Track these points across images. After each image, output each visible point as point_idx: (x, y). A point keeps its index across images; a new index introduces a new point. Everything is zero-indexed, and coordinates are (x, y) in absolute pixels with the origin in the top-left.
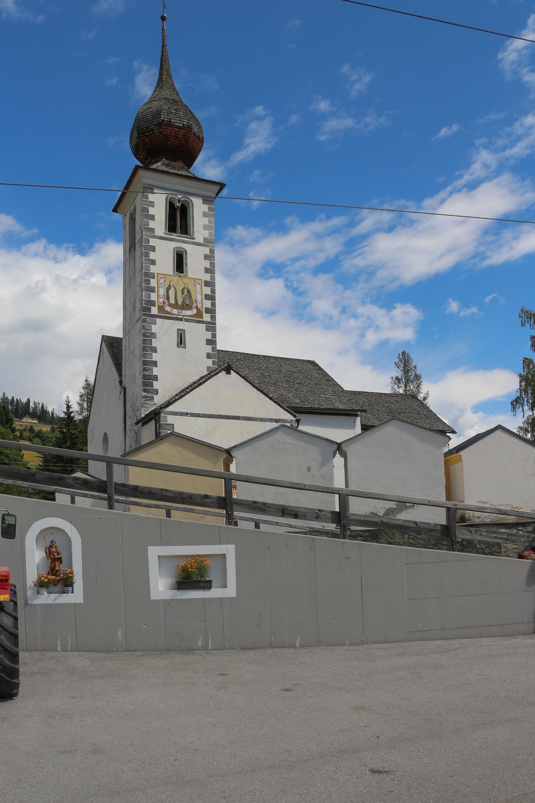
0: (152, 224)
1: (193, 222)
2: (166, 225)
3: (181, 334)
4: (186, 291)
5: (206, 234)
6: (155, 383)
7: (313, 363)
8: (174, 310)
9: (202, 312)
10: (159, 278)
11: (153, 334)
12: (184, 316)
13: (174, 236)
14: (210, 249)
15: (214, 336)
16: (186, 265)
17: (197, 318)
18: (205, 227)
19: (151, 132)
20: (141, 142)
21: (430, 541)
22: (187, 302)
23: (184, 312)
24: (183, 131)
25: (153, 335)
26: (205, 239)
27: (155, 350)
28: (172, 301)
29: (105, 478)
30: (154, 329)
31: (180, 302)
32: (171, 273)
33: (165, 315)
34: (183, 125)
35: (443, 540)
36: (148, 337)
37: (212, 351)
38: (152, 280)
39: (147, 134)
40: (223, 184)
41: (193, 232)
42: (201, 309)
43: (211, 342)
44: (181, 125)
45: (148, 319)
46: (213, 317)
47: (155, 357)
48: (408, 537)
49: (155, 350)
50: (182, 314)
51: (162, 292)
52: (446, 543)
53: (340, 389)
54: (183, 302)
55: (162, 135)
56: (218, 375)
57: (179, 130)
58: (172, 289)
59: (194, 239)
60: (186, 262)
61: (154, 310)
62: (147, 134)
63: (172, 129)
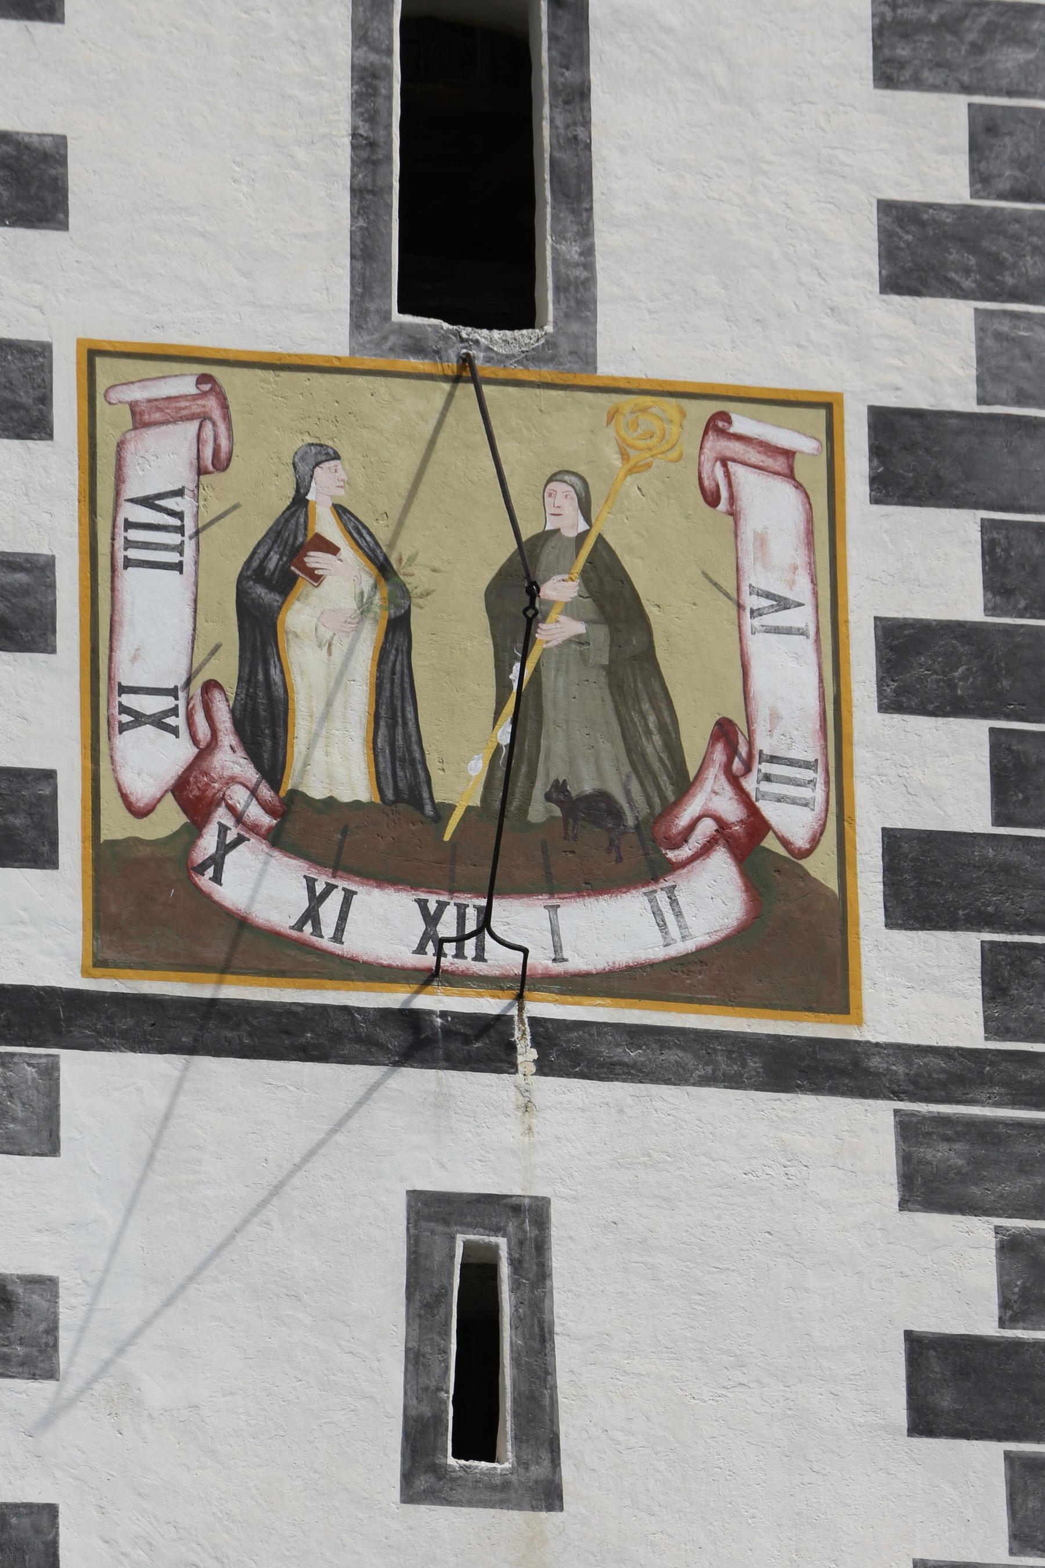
3: (480, 1275)
9: (839, 910)
10: (112, 422)
12: (522, 985)
16: (577, 189)
22: (583, 754)
23: (519, 918)
28: (335, 762)
29: (170, 795)
31: (460, 777)
32: (322, 322)
42: (821, 867)
50: (501, 960)
51: (164, 628)
54: (510, 769)
58: (342, 580)
60: (578, 144)
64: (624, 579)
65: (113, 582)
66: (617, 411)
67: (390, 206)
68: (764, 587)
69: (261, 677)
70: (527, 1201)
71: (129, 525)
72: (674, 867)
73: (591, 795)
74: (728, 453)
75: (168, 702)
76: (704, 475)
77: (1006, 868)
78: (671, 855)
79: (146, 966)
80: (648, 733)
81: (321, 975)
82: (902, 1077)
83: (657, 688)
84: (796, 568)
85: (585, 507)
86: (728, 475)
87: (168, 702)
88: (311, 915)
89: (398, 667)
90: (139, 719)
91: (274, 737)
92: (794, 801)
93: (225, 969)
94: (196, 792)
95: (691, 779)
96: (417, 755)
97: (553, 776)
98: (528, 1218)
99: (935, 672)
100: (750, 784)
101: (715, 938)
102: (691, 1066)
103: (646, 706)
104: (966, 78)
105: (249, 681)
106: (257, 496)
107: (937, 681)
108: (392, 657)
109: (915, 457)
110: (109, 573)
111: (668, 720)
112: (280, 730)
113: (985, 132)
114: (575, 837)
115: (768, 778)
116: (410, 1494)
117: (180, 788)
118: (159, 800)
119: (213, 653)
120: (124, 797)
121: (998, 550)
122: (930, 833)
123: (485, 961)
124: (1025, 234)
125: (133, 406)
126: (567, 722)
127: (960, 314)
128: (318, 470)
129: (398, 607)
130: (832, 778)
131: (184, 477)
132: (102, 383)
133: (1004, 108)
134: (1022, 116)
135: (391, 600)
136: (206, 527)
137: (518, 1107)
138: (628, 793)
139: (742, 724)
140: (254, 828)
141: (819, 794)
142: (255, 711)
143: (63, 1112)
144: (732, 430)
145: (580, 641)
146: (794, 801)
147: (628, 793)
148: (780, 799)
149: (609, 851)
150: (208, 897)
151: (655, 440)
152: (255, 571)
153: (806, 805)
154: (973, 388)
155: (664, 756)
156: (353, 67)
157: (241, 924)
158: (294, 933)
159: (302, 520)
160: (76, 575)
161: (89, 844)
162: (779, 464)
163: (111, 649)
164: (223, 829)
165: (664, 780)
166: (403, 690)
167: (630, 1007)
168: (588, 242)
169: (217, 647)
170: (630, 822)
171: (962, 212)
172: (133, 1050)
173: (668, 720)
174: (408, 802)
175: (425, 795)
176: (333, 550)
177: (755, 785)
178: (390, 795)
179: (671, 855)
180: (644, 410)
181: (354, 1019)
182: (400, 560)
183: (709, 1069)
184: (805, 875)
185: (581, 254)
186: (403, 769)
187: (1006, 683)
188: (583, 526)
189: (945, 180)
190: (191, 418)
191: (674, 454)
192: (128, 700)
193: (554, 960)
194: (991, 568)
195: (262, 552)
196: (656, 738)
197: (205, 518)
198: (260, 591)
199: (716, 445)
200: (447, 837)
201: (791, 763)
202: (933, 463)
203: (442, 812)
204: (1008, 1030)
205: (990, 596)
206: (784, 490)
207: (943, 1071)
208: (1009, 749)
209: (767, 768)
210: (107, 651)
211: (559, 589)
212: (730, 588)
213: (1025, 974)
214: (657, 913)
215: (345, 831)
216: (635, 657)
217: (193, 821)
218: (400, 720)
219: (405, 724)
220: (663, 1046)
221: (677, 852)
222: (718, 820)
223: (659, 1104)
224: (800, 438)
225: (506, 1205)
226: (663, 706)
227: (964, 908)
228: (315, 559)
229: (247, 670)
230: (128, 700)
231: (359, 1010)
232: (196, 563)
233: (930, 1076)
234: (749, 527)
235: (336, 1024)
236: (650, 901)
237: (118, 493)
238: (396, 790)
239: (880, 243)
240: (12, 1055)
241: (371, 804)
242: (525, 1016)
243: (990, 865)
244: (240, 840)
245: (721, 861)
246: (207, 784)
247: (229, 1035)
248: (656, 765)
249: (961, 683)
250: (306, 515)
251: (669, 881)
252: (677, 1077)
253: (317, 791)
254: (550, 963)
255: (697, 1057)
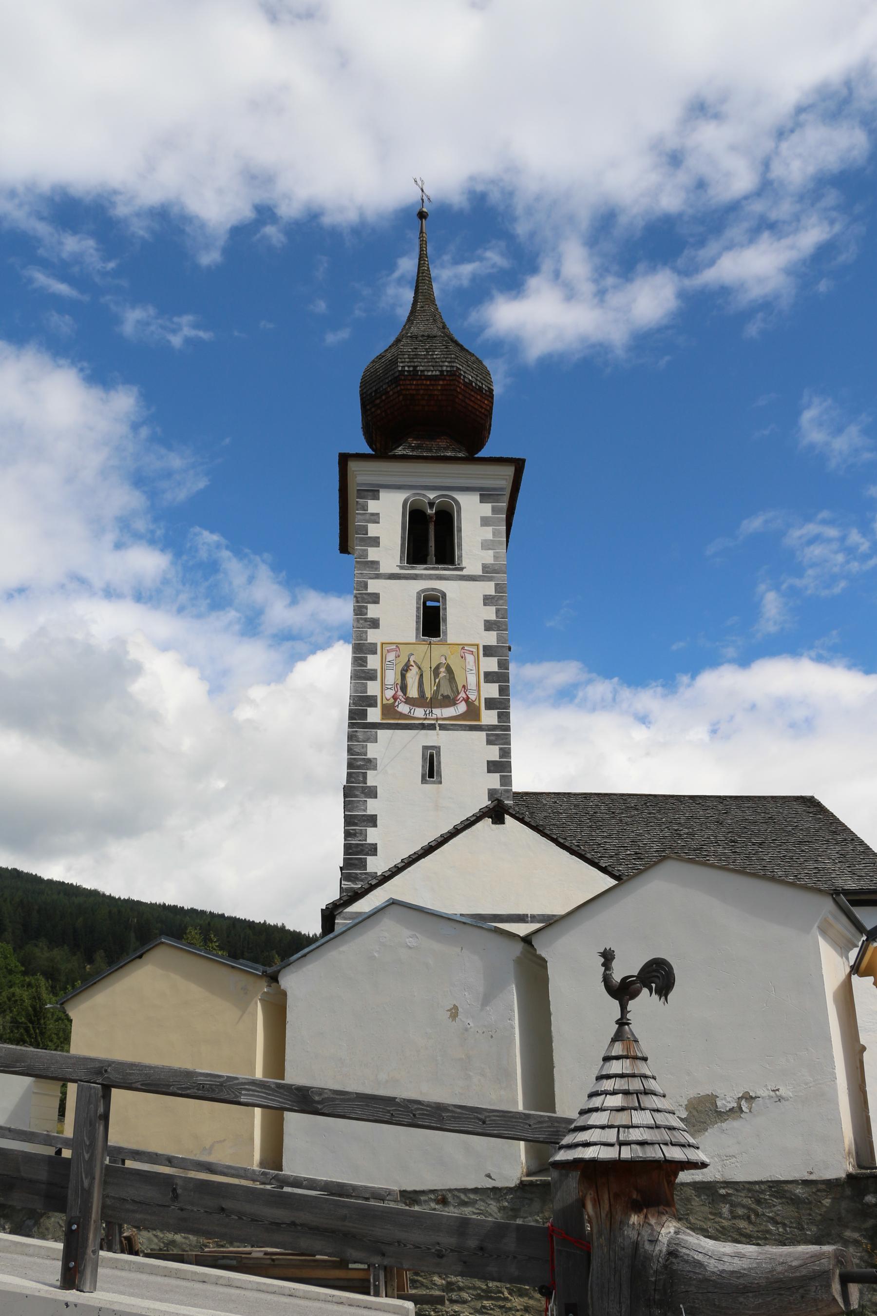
0: (373, 554)
1: (460, 538)
2: (402, 552)
3: (432, 756)
4: (442, 670)
5: (488, 557)
6: (370, 859)
7: (810, 803)
8: (418, 710)
9: (479, 708)
11: (369, 761)
12: (437, 719)
13: (420, 570)
14: (496, 585)
15: (506, 753)
16: (445, 620)
17: (470, 720)
18: (375, 518)
19: (384, 397)
20: (369, 418)
21: (802, 1229)
22: (446, 690)
23: (435, 711)
24: (441, 383)
25: (371, 764)
26: (485, 567)
27: (372, 793)
28: (413, 693)
30: (372, 751)
33: (394, 721)
34: (442, 371)
35: (846, 1227)
36: (359, 767)
37: (501, 785)
38: (370, 658)
39: (378, 401)
40: (519, 459)
41: (460, 557)
42: (477, 703)
43: (501, 766)
44: (438, 373)
45: (361, 733)
46: (504, 716)
47: (372, 807)
48: (731, 1212)
49: (372, 793)
50: (434, 716)
51: (391, 677)
52: (856, 1235)
53: (861, 849)
55: (401, 398)
56: (474, 828)
57: (433, 382)
58: (414, 670)
59: (462, 569)
61: (374, 715)
62: (378, 401)
63: (419, 382)
93: (399, 719)
95: (480, 455)
98: (438, 748)
109: (488, 651)
113: (497, 611)
116: (422, 783)
127: (495, 633)
157: (401, 713)
189: (493, 617)
211: (442, 670)
224: (474, 650)
249: (17, 982)
252: (457, 730)
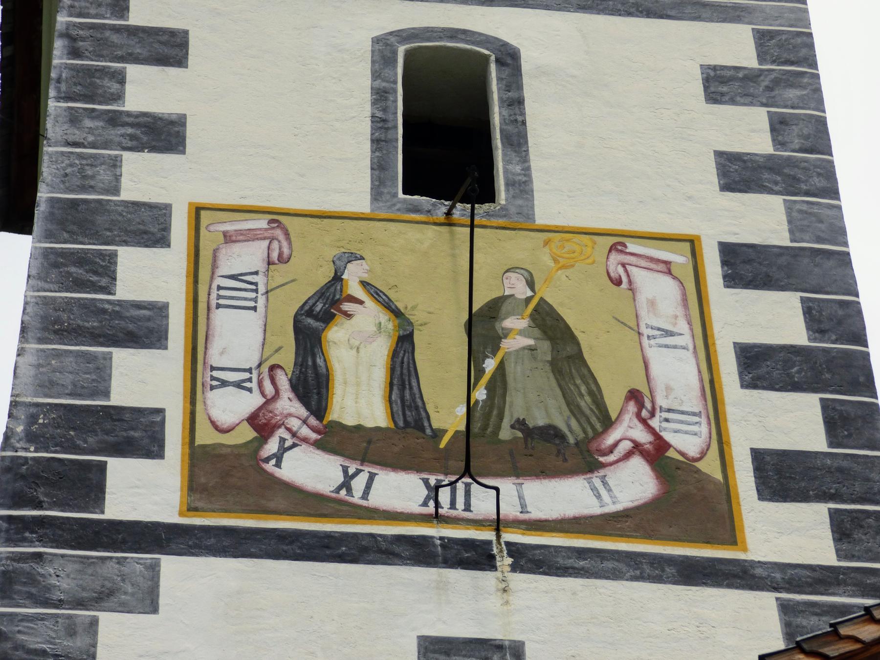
12: (498, 524)
22: (536, 401)
31: (448, 415)
42: (711, 467)
51: (241, 337)
64: (559, 319)
65: (208, 315)
66: (550, 240)
67: (397, 148)
68: (655, 324)
69: (310, 363)
70: (507, 643)
71: (219, 288)
72: (603, 466)
73: (543, 426)
74: (626, 261)
75: (246, 375)
76: (611, 271)
77: (840, 470)
78: (601, 459)
79: (226, 511)
80: (581, 395)
81: (352, 517)
82: (780, 580)
83: (586, 372)
84: (676, 317)
85: (531, 284)
86: (626, 271)
87: (246, 375)
88: (346, 485)
89: (406, 359)
90: (224, 383)
91: (319, 393)
92: (686, 433)
94: (264, 421)
96: (420, 404)
97: (515, 416)
99: (778, 369)
100: (655, 423)
101: (636, 504)
102: (624, 570)
103: (578, 382)
104: (764, 101)
105: (301, 365)
106: (307, 278)
107: (780, 374)
108: (401, 355)
110: (206, 311)
111: (595, 389)
112: (324, 391)
114: (533, 448)
115: (667, 420)
117: (252, 419)
118: (238, 425)
119: (277, 351)
120: (213, 423)
121: (814, 312)
122: (784, 451)
123: (470, 511)
124: (812, 168)
125: (225, 234)
126: (524, 389)
128: (349, 265)
129: (405, 330)
130: (713, 421)
131: (261, 266)
132: (204, 222)
133: (790, 114)
134: (802, 117)
135: (400, 326)
136: (272, 290)
137: (498, 590)
138: (569, 426)
139: (645, 391)
140: (305, 440)
141: (704, 429)
142: (306, 380)
143: (162, 590)
144: (627, 251)
145: (531, 349)
146: (686, 433)
147: (569, 426)
148: (676, 431)
149: (557, 456)
150: (271, 476)
151: (576, 254)
152: (307, 311)
153: (695, 434)
154: (787, 235)
155: (593, 407)
156: (372, 88)
158: (334, 495)
159: (339, 288)
160: (183, 311)
161: (187, 447)
162: (661, 267)
163: (206, 348)
164: (282, 440)
165: (594, 420)
166: (409, 371)
167: (578, 538)
168: (526, 165)
169: (280, 348)
170: (572, 440)
171: (770, 157)
172: (215, 556)
173: (595, 389)
174: (414, 428)
175: (426, 424)
176: (361, 302)
177: (658, 424)
178: (401, 423)
179: (601, 459)
180: (568, 240)
181: (376, 541)
182: (406, 308)
183: (638, 572)
184: (698, 471)
185: (522, 170)
186: (411, 411)
187: (828, 376)
188: (529, 293)
190: (265, 238)
191: (590, 261)
192: (215, 374)
193: (521, 512)
194: (810, 320)
195: (311, 302)
196: (588, 399)
197: (273, 285)
198: (310, 321)
199: (615, 257)
200: (442, 445)
201: (683, 413)
202: (765, 269)
203: (438, 434)
204: (853, 556)
205: (811, 333)
206: (667, 280)
207: (809, 577)
208: (834, 409)
209: (665, 415)
210: (203, 349)
212: (633, 324)
213: (862, 527)
214: (594, 489)
215: (369, 442)
216: (569, 357)
217: (262, 436)
218: (407, 387)
219: (411, 388)
220: (603, 559)
221: (605, 458)
222: (633, 441)
223: (601, 590)
225: (491, 645)
226: (591, 382)
227: (813, 490)
228: (347, 306)
229: (300, 359)
230: (215, 374)
231: (380, 536)
232: (266, 307)
233: (800, 579)
234: (642, 298)
235: (363, 543)
236: (589, 483)
237: (213, 273)
238: (405, 421)
239: (718, 169)
240: (126, 558)
241: (388, 429)
242: (502, 541)
243: (829, 468)
244: (294, 445)
245: (638, 464)
246: (272, 417)
247: (285, 548)
248: (588, 412)
250: (342, 286)
251: (602, 472)
252: (615, 575)
253: (350, 421)
254: (518, 514)
255: (629, 565)
